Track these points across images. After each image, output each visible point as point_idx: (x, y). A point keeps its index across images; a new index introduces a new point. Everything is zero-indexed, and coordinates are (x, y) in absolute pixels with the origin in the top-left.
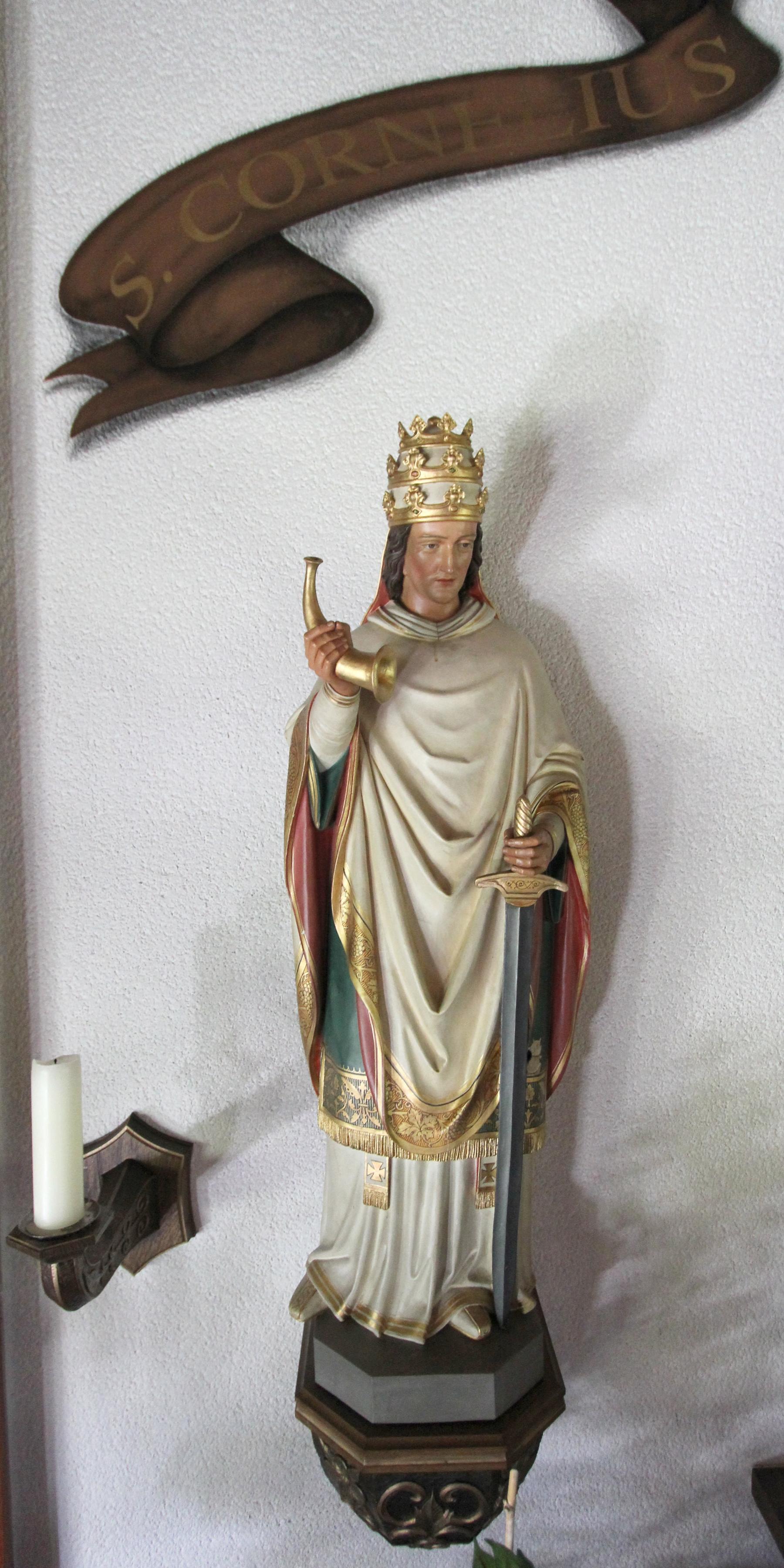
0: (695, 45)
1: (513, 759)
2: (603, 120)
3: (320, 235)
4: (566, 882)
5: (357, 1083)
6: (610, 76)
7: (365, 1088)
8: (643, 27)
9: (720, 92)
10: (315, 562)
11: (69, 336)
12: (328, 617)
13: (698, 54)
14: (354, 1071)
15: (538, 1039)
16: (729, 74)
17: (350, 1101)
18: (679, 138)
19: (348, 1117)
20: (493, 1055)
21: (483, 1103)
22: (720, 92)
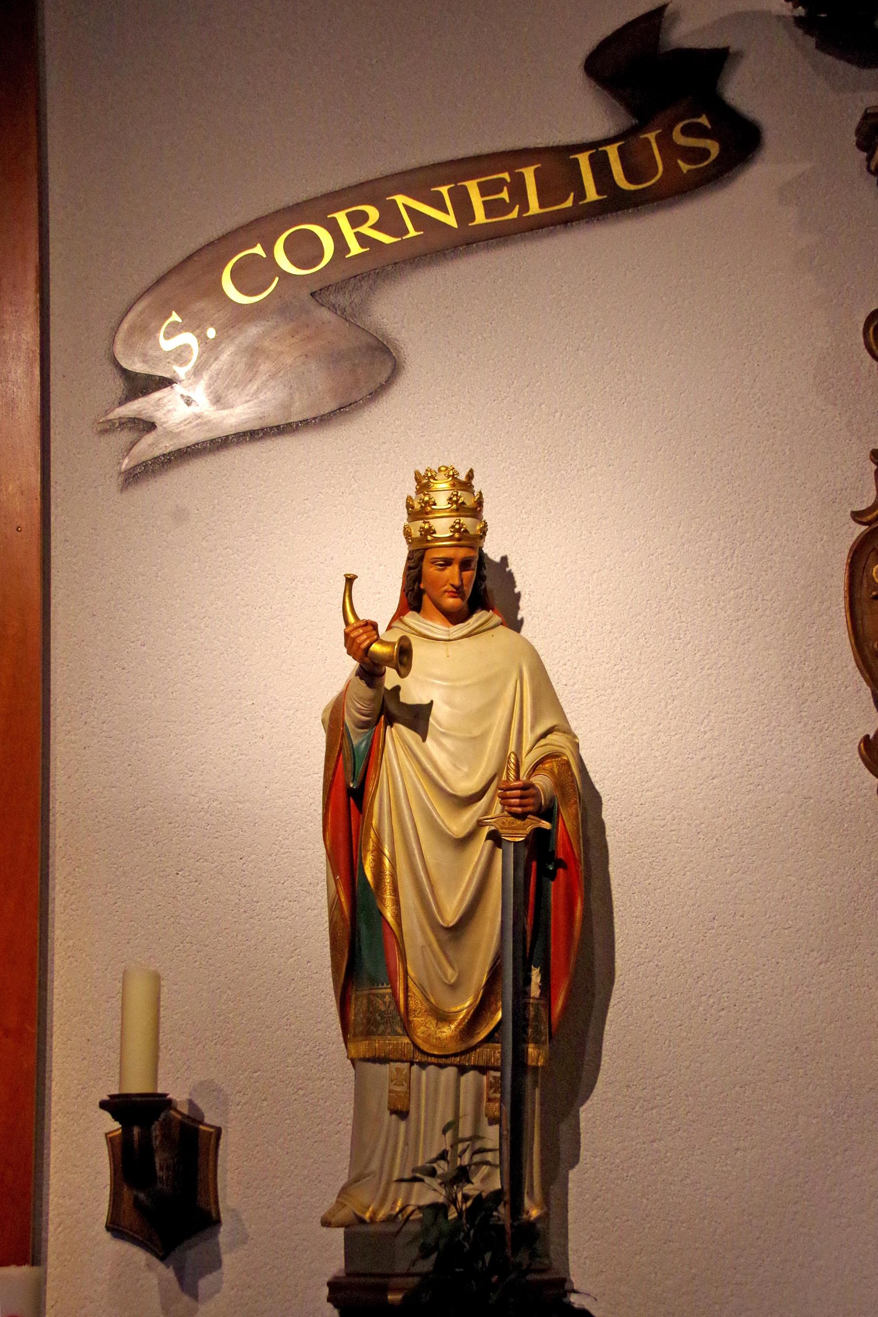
0: (680, 125)
1: (509, 734)
2: (599, 192)
3: (347, 296)
4: (550, 821)
5: (384, 996)
6: (605, 153)
7: (389, 1000)
8: (632, 109)
9: (706, 163)
10: (350, 580)
11: (122, 385)
12: (361, 619)
13: (685, 131)
14: (380, 986)
15: (537, 968)
16: (714, 148)
17: (377, 1014)
18: (671, 205)
19: (375, 1030)
20: (495, 973)
21: (489, 1014)
22: (706, 163)
